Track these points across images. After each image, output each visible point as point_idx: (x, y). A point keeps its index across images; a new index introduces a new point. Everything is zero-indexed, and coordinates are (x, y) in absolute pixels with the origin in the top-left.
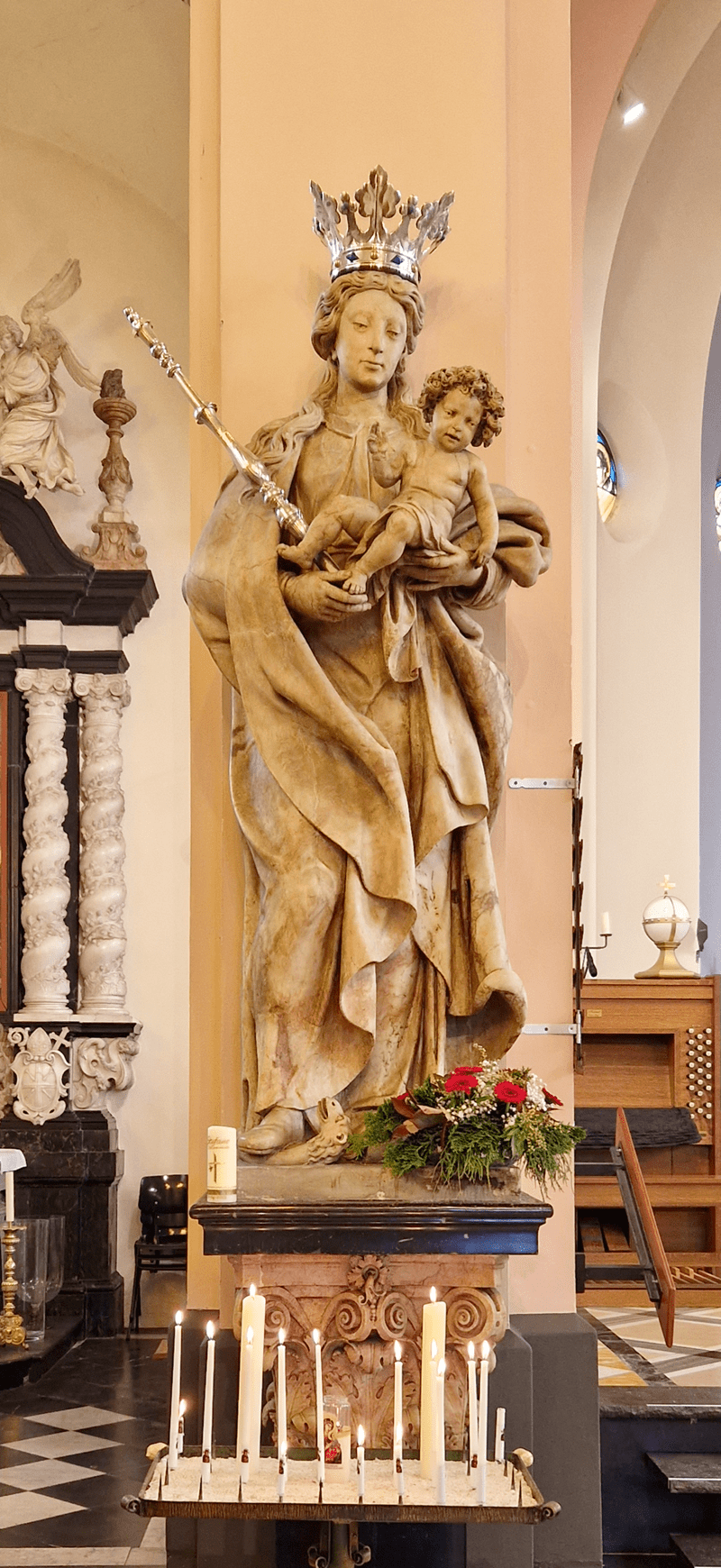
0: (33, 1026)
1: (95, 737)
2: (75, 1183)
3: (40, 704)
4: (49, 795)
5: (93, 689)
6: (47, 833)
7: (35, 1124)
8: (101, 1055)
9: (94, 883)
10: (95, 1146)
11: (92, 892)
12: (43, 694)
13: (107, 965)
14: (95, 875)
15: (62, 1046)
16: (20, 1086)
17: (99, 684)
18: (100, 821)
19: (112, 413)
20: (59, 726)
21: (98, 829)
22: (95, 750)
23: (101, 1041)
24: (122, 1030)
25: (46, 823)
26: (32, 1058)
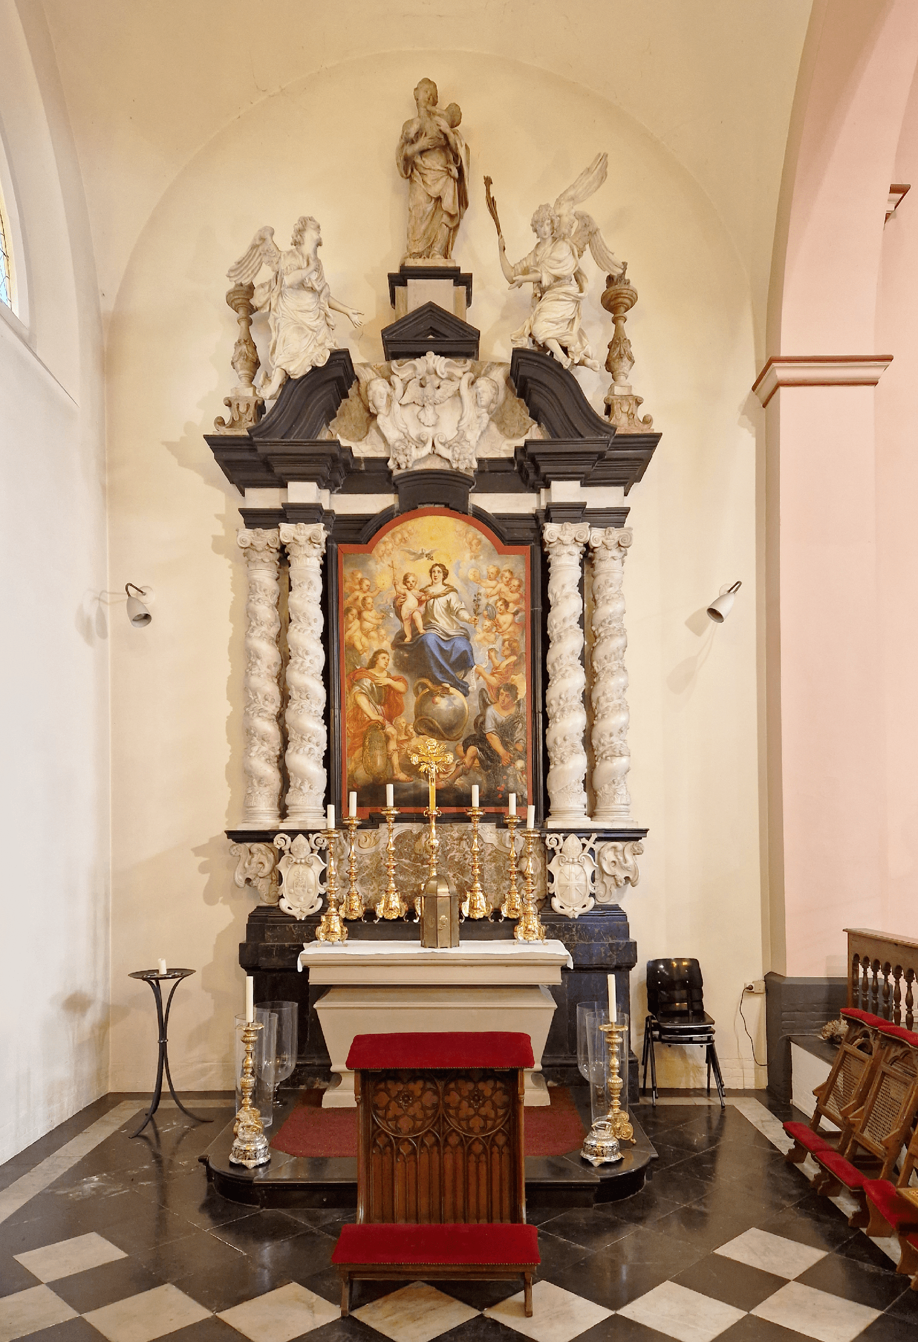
5: (605, 541)
6: (571, 665)
8: (619, 857)
9: (607, 709)
11: (606, 716)
13: (619, 778)
14: (607, 701)
15: (591, 849)
16: (557, 885)
17: (611, 536)
19: (620, 300)
20: (575, 573)
23: (619, 845)
24: (634, 836)
26: (567, 859)
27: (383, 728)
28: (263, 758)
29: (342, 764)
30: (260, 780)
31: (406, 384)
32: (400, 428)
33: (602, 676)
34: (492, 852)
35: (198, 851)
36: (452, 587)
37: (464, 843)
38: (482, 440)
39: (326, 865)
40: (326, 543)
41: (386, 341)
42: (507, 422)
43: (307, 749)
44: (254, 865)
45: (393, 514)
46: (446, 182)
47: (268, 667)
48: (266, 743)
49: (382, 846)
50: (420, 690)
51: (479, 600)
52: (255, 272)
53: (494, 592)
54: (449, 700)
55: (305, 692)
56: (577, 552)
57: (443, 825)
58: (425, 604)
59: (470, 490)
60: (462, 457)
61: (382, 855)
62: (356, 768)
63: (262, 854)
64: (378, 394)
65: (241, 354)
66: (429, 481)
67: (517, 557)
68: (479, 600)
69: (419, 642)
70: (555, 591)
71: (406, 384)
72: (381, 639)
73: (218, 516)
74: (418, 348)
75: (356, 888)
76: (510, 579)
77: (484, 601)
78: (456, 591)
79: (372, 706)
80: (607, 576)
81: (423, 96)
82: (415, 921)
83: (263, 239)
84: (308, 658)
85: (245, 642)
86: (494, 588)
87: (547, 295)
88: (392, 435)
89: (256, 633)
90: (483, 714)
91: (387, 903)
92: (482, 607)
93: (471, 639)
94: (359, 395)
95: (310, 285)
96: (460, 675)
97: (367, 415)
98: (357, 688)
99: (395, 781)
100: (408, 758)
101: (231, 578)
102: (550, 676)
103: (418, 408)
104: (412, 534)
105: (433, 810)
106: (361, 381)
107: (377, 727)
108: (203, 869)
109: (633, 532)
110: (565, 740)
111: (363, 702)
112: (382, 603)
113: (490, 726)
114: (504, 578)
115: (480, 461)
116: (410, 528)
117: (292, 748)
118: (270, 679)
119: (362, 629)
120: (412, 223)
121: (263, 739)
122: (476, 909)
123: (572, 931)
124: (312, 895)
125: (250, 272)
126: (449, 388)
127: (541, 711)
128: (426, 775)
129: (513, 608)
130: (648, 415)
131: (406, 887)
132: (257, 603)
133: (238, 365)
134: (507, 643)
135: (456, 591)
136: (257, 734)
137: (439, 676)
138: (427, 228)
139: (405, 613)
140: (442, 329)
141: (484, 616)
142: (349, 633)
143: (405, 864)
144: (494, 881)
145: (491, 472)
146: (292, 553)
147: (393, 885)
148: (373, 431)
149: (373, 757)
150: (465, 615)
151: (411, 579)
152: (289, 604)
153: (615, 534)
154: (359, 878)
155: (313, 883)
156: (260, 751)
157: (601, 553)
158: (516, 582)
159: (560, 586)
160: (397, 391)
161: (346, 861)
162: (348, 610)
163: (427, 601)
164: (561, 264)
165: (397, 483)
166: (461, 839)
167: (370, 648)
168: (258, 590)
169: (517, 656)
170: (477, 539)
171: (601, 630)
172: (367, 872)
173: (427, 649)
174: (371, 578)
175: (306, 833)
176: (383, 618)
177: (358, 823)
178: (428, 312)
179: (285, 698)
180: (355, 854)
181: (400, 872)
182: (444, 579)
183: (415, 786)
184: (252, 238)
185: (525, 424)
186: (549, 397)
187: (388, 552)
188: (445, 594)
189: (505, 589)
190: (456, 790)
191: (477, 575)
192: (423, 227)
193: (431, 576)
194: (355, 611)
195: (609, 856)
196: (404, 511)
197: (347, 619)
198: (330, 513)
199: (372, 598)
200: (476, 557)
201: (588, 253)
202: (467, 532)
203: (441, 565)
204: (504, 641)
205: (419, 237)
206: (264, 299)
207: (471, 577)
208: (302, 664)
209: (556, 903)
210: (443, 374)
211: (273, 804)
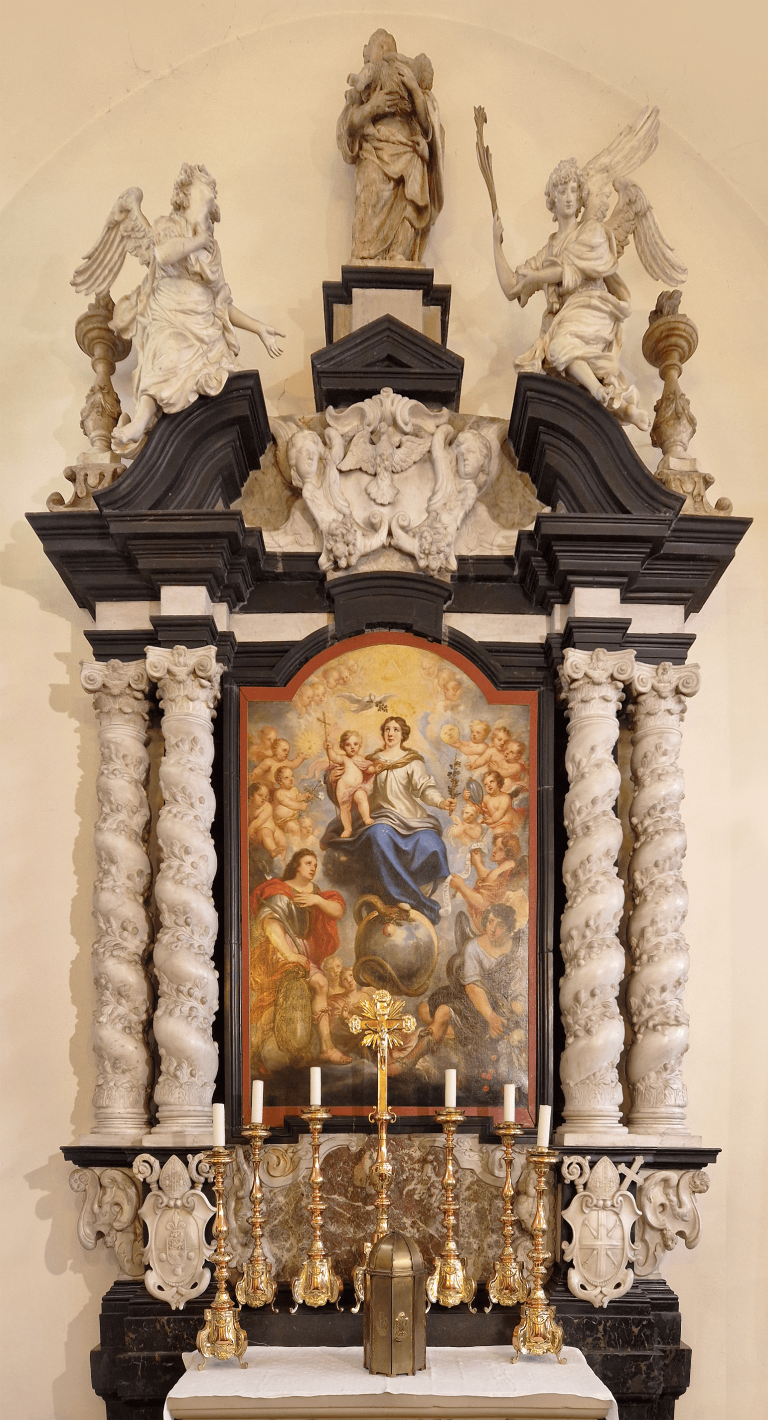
0: (597, 1153)
1: (657, 747)
2: (648, 1401)
3: (594, 698)
4: (606, 822)
5: (656, 684)
6: (604, 874)
7: (597, 1306)
9: (657, 946)
10: (661, 1338)
11: (656, 959)
12: (599, 684)
13: (673, 1062)
14: (658, 934)
15: (633, 1183)
16: (577, 1246)
17: (666, 677)
18: (665, 861)
20: (611, 730)
21: (661, 872)
22: (655, 766)
23: (673, 1175)
25: (603, 859)
27: (307, 974)
28: (119, 1026)
29: (243, 1036)
30: (116, 1062)
31: (348, 441)
32: (338, 506)
33: (650, 894)
34: (472, 1183)
35: (33, 1179)
36: (414, 752)
37: (429, 1169)
38: (464, 529)
39: (215, 1209)
40: (222, 684)
41: (318, 372)
42: (504, 506)
43: (186, 1009)
44: (106, 1208)
45: (325, 641)
46: (410, 161)
47: (129, 877)
48: (123, 1001)
49: (303, 1173)
50: (364, 913)
51: (459, 773)
52: (115, 269)
53: (481, 761)
54: (408, 929)
55: (186, 917)
56: (614, 695)
57: (397, 1136)
58: (372, 779)
59: (445, 606)
60: (434, 549)
61: (303, 1189)
62: (263, 1042)
63: (119, 1188)
64: (304, 454)
65: (93, 406)
66: (383, 591)
67: (518, 708)
68: (459, 773)
69: (364, 838)
70: (578, 757)
71: (348, 441)
72: (305, 833)
73: (59, 656)
74: (367, 385)
75: (265, 1249)
76: (506, 742)
77: (464, 775)
78: (421, 758)
79: (289, 939)
80: (660, 738)
81: (375, 53)
82: (355, 1310)
83: (125, 211)
84: (189, 859)
85: (95, 840)
86: (481, 754)
87: (570, 301)
88: (326, 516)
89: (111, 823)
90: (460, 953)
91: (310, 1278)
92: (462, 785)
93: (444, 834)
94: (276, 463)
95: (197, 268)
96: (427, 889)
97: (287, 493)
98: (267, 911)
99: (324, 1064)
100: (344, 1023)
101: (78, 747)
102: (569, 892)
103: (366, 478)
104: (355, 672)
105: (383, 1111)
106: (279, 441)
107: (299, 973)
108: (43, 1210)
109: (700, 671)
110: (593, 994)
111: (276, 935)
112: (307, 777)
113: (471, 972)
114: (496, 741)
115: (461, 560)
116: (351, 662)
117: (163, 1008)
118: (131, 896)
119: (275, 817)
120: (361, 211)
121: (120, 994)
122: (449, 1288)
123: (598, 1331)
124: (195, 1263)
125: (107, 271)
126: (414, 449)
127: (551, 948)
128: (373, 1051)
129: (509, 785)
130: (724, 499)
131: (340, 1243)
132: (111, 776)
133: (90, 424)
134: (500, 840)
135: (421, 758)
136: (110, 986)
137: (394, 891)
138: (383, 224)
139: (342, 792)
140: (405, 358)
141: (464, 797)
142: (255, 824)
143: (339, 1205)
144: (475, 1236)
145: (478, 579)
146: (167, 696)
147: (320, 1245)
148: (297, 515)
149: (290, 1021)
150: (435, 796)
151: (352, 740)
152: (161, 774)
153: (673, 674)
154: (268, 1228)
155: (196, 1242)
156: (115, 1014)
157: (649, 702)
158: (514, 747)
159: (589, 747)
160: (334, 450)
161: (246, 1201)
162: (255, 788)
163: (377, 774)
164: (593, 255)
165: (333, 591)
166: (424, 1161)
167: (287, 848)
168: (114, 757)
169: (515, 860)
170: (455, 680)
171: (647, 822)
172: (280, 1218)
173: (375, 850)
174: (291, 738)
175: (183, 1153)
176: (308, 800)
177: (264, 1134)
178: (384, 330)
179: (155, 926)
180: (260, 1190)
181: (331, 1219)
182: (404, 740)
183: (355, 1071)
184: (110, 210)
185: (530, 510)
186: (575, 456)
187: (317, 698)
188: (405, 764)
189: (498, 757)
190: (417, 1078)
191: (455, 733)
192: (376, 223)
193: (383, 735)
194: (264, 790)
195: (656, 1194)
196: (344, 637)
197: (253, 801)
198: (229, 636)
199: (292, 769)
200: (453, 708)
201: (630, 249)
202: (440, 670)
203: (398, 719)
204: (495, 838)
205: (370, 236)
206: (128, 317)
207: (445, 738)
208: (178, 870)
209: (575, 1278)
210: (406, 424)
211: (137, 1102)
